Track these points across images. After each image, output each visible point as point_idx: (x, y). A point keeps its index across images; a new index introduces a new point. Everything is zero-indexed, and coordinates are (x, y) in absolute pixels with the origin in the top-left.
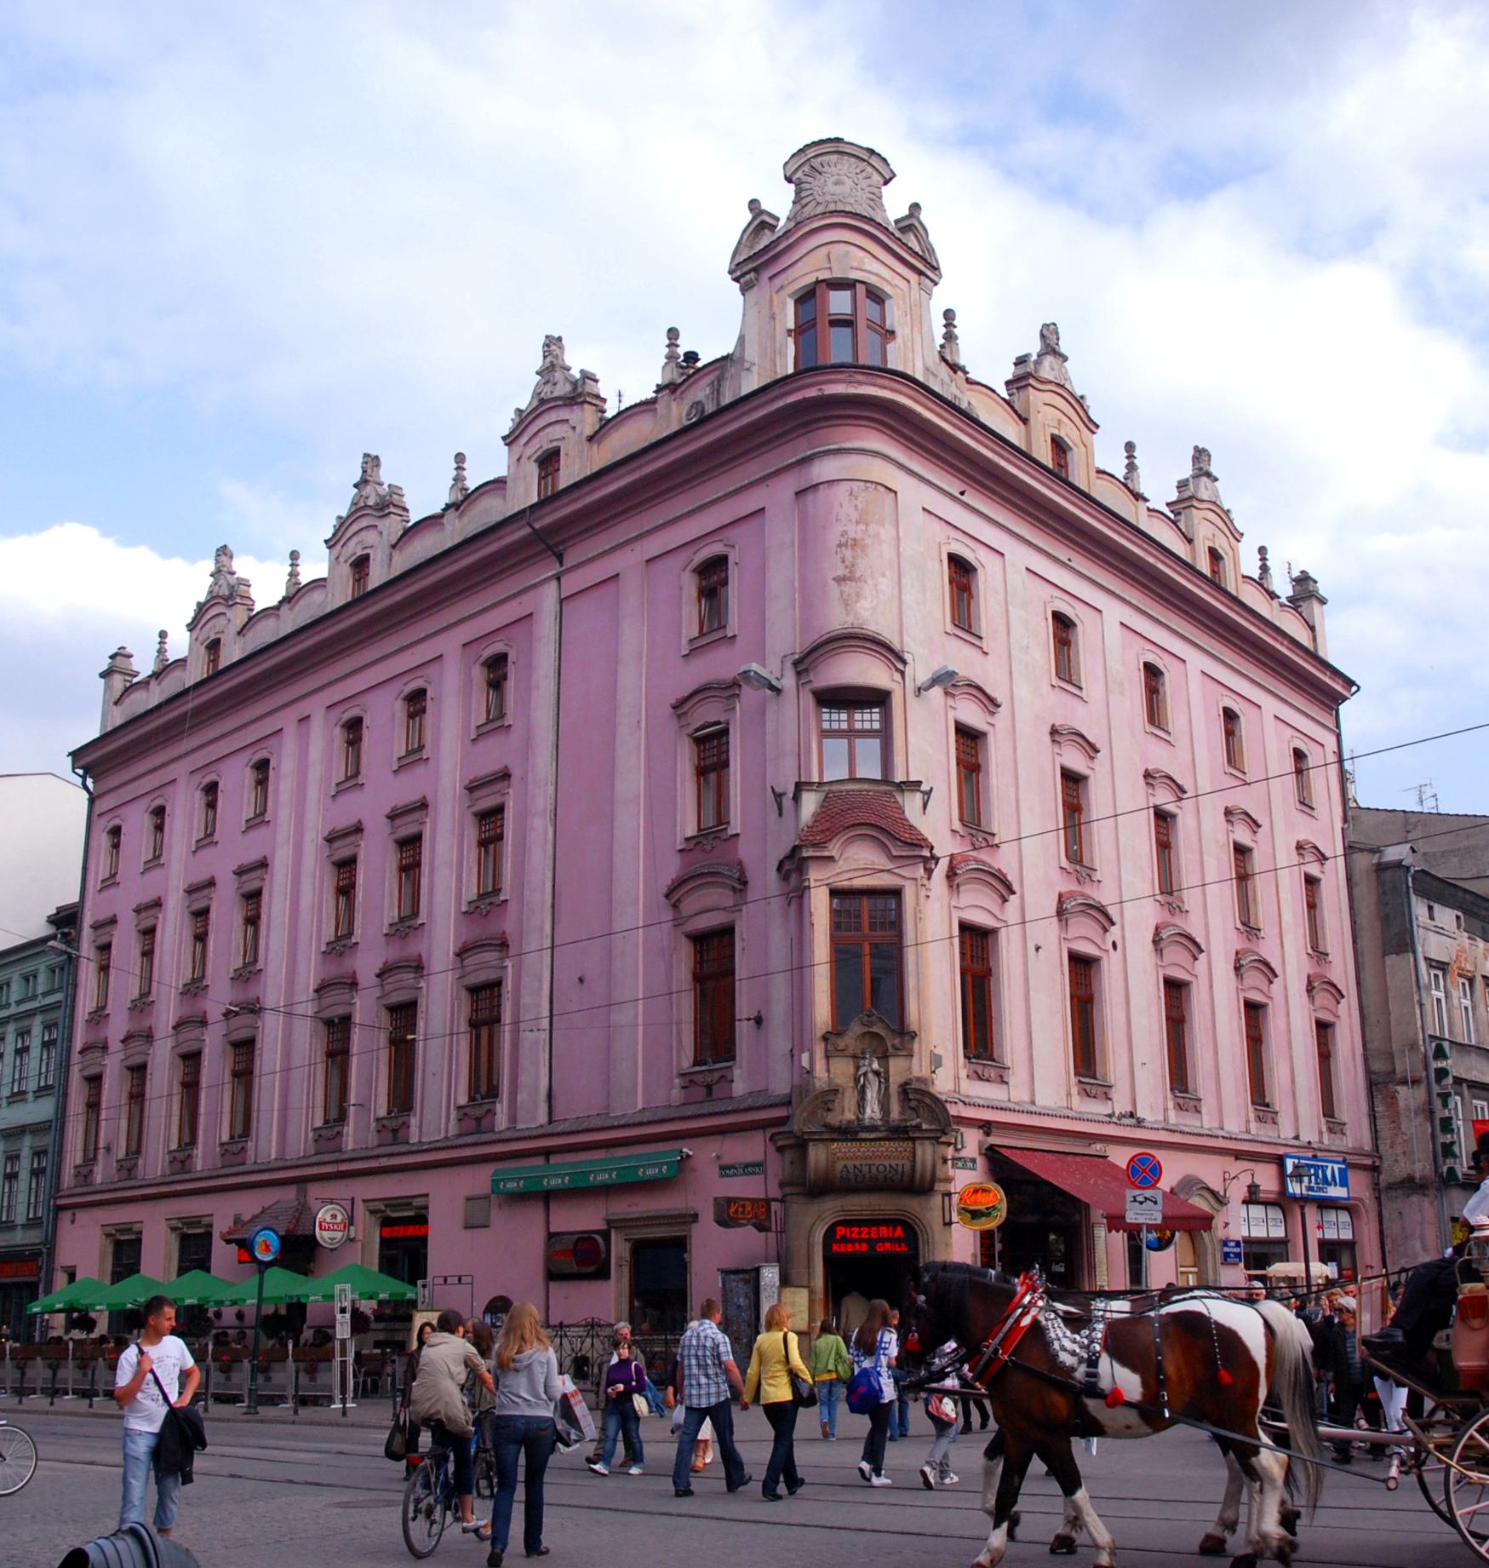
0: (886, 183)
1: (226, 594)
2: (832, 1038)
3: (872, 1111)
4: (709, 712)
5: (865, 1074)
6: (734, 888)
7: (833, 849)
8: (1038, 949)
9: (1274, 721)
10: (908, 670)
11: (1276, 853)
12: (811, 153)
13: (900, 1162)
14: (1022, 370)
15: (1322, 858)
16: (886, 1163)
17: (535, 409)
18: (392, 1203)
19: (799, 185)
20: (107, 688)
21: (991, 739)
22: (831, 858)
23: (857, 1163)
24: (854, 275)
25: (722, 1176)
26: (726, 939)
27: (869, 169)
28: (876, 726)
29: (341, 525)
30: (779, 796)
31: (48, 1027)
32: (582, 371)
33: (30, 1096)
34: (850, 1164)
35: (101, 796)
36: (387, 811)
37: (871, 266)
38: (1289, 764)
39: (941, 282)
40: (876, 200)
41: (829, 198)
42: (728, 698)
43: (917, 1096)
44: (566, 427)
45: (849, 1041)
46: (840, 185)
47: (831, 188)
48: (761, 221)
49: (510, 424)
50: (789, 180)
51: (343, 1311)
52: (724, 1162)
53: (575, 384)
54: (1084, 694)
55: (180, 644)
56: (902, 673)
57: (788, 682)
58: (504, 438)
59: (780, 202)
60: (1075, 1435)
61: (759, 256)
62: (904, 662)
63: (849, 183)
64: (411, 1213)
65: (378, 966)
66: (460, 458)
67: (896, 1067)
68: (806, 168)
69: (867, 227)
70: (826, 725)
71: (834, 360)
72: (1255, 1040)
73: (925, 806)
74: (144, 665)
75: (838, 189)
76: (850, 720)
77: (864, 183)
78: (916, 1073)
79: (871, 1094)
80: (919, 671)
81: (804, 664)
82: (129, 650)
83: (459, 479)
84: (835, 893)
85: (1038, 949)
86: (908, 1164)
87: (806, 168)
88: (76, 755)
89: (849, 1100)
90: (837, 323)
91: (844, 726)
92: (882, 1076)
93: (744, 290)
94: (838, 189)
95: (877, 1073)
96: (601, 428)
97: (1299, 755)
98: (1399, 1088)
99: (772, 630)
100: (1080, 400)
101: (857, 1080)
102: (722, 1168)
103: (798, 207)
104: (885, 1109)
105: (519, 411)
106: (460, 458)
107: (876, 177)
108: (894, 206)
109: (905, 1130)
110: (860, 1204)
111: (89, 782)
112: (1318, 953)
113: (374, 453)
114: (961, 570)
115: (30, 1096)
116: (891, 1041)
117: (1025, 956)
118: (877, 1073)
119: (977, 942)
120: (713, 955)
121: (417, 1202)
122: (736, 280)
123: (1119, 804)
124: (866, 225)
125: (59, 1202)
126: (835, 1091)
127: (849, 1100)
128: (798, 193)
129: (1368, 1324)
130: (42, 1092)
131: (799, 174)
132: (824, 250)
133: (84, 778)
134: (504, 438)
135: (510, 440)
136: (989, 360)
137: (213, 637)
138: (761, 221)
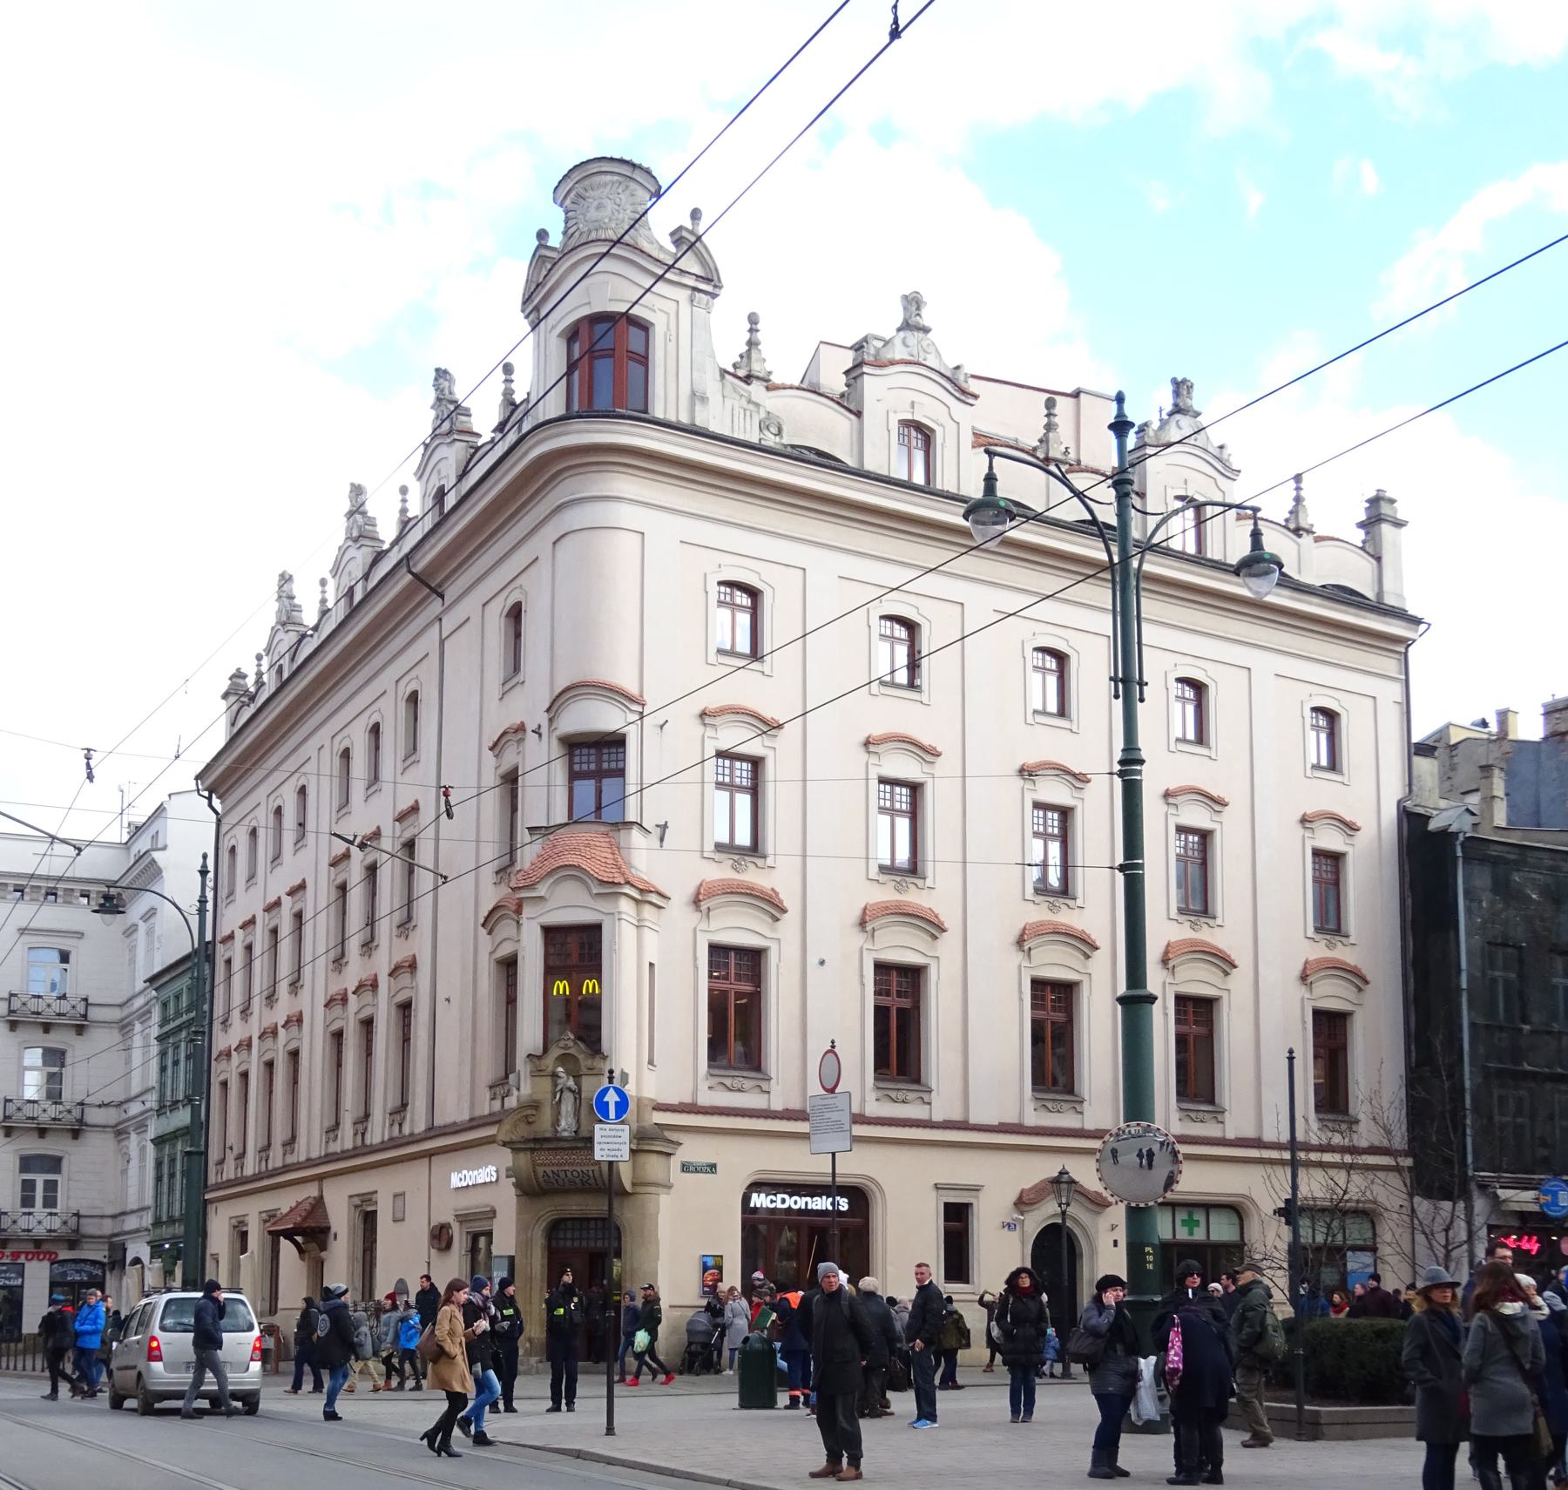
7: (542, 890)
12: (576, 176)
23: (555, 1169)
27: (633, 185)
34: (548, 1169)
35: (226, 813)
39: (723, 292)
41: (591, 226)
45: (549, 1061)
46: (610, 210)
51: (137, 1261)
54: (925, 699)
60: (863, 1416)
63: (609, 205)
66: (753, 320)
70: (577, 768)
73: (662, 840)
76: (599, 761)
79: (567, 1106)
89: (547, 1113)
91: (593, 767)
92: (577, 1093)
107: (642, 195)
108: (663, 221)
110: (576, 1206)
111: (216, 802)
116: (585, 1062)
127: (547, 1113)
129: (352, 1362)
133: (210, 799)
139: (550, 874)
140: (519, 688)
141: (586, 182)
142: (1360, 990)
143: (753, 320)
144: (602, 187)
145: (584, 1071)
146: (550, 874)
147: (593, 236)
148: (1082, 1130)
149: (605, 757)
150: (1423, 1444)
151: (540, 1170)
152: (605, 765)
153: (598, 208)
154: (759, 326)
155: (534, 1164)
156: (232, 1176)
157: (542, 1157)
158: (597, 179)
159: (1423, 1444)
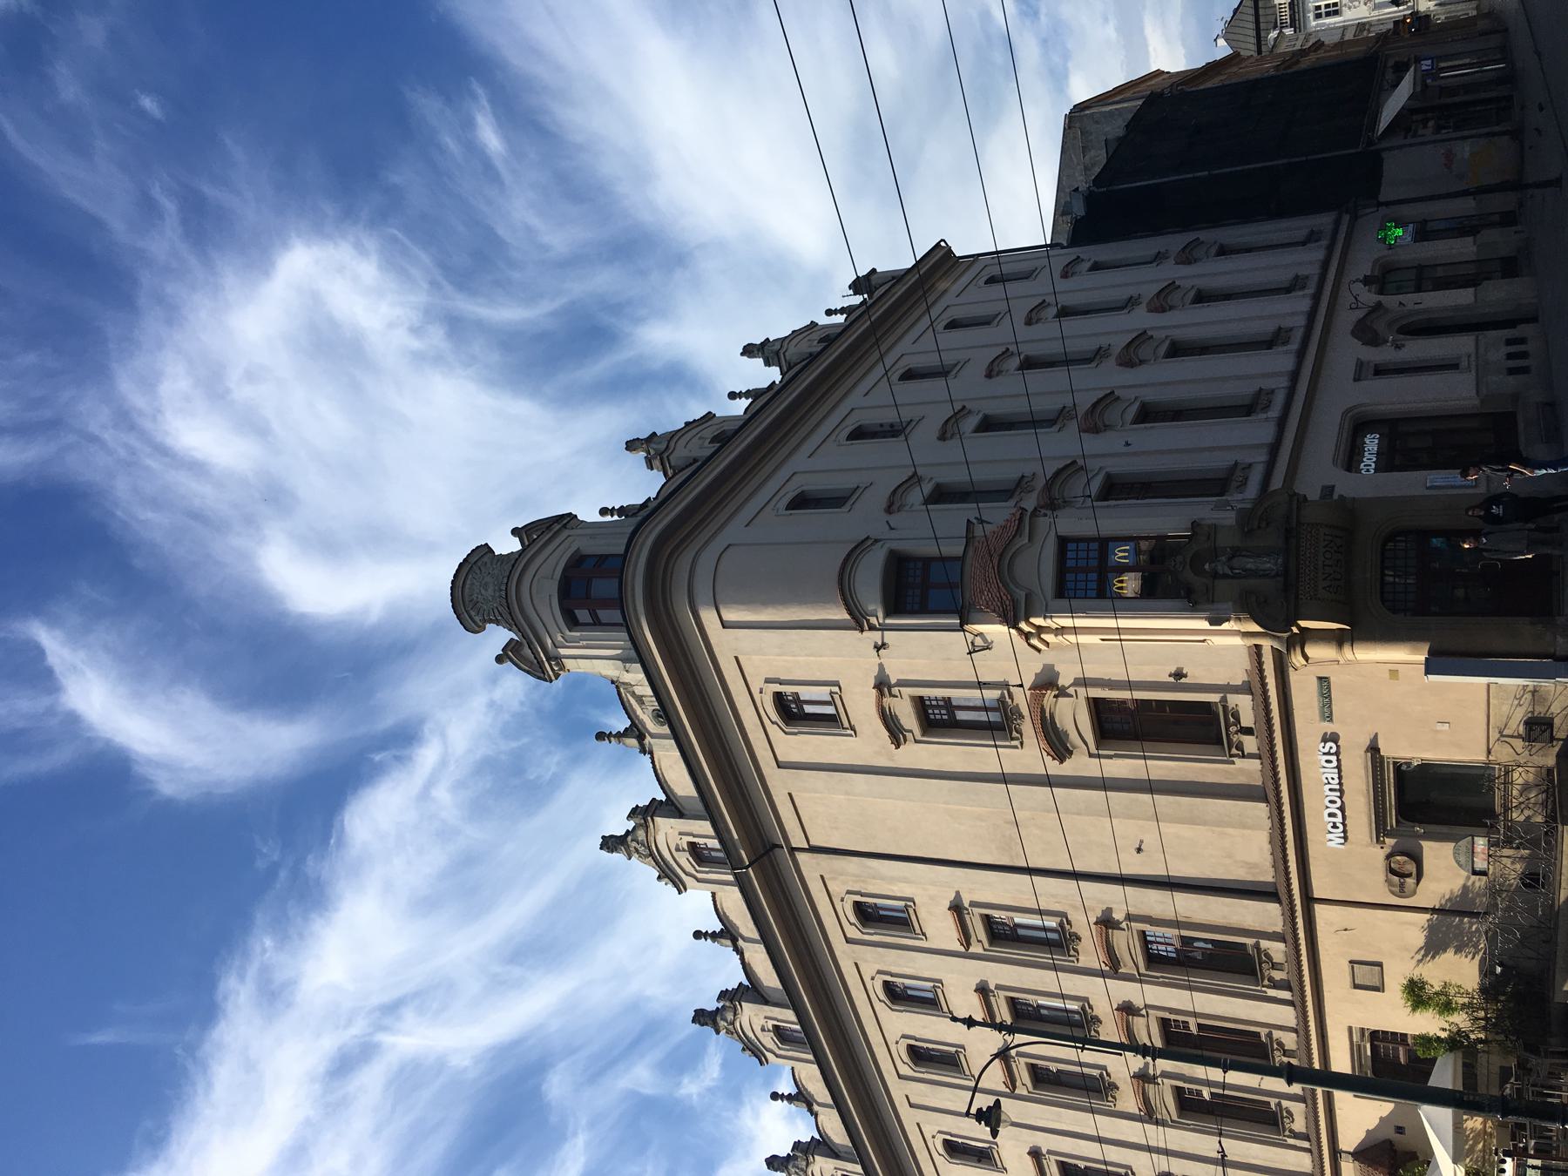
3: (1268, 564)
5: (1232, 569)
8: (1127, 444)
10: (874, 535)
15: (1078, 260)
19: (485, 621)
21: (941, 480)
32: (629, 817)
37: (554, 561)
38: (999, 287)
43: (1249, 521)
56: (876, 541)
59: (499, 636)
66: (698, 935)
72: (1227, 296)
83: (714, 936)
85: (1127, 444)
92: (1236, 552)
95: (1230, 559)
97: (991, 280)
98: (1423, 843)
100: (687, 424)
101: (1234, 577)
106: (698, 935)
107: (485, 559)
112: (1159, 258)
114: (802, 502)
117: (1135, 454)
119: (1115, 489)
123: (1009, 395)
128: (491, 621)
131: (477, 619)
135: (680, 887)
139: (1005, 585)
146: (1005, 585)
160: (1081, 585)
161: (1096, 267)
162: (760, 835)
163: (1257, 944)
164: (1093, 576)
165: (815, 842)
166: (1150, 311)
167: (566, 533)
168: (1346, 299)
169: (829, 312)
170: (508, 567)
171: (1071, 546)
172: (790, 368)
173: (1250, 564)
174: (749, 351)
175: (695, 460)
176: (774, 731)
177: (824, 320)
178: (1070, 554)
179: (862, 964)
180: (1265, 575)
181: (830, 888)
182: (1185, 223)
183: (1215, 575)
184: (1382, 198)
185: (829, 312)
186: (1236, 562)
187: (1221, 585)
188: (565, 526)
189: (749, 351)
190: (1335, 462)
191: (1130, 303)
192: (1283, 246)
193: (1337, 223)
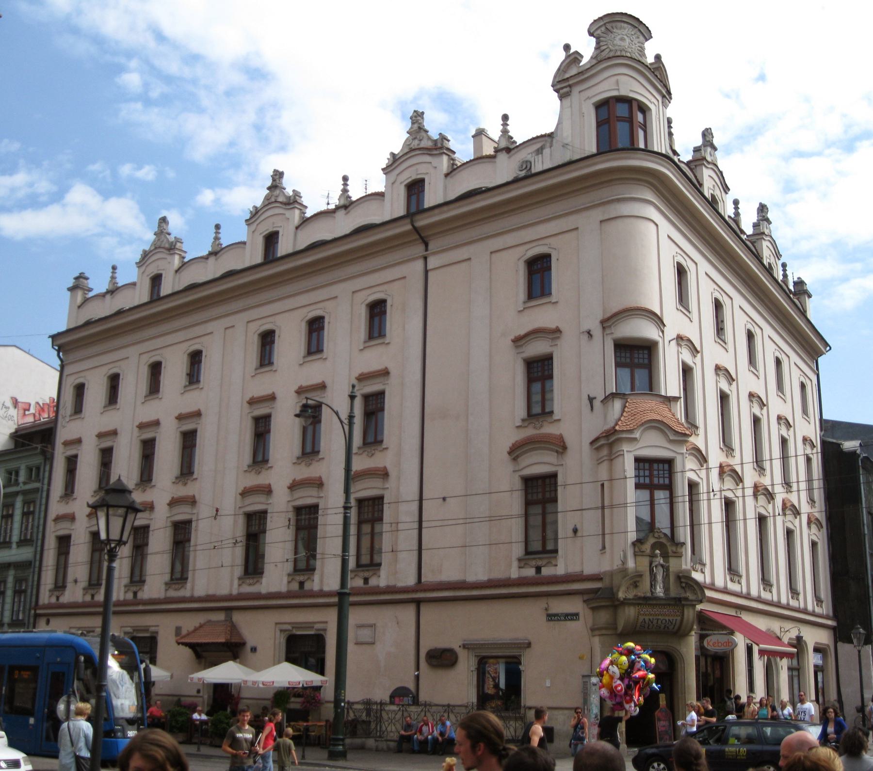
0: (647, 40)
1: (164, 244)
2: (639, 544)
3: (659, 591)
4: (537, 348)
6: (557, 452)
7: (637, 435)
9: (795, 368)
11: (797, 448)
13: (675, 618)
14: (698, 156)
15: (813, 446)
16: (667, 618)
17: (406, 154)
18: (136, 629)
19: (598, 38)
20: (73, 299)
22: (635, 439)
23: (651, 618)
24: (632, 95)
25: (549, 620)
26: (553, 480)
27: (639, 33)
28: (636, 361)
29: (257, 213)
30: (591, 400)
31: (26, 503)
33: (14, 545)
34: (647, 618)
36: (296, 388)
40: (642, 51)
41: (617, 48)
42: (553, 339)
44: (428, 166)
45: (647, 547)
46: (623, 39)
47: (617, 42)
48: (573, 58)
49: (387, 161)
50: (591, 34)
52: (550, 612)
53: (435, 141)
55: (128, 275)
56: (663, 332)
57: (597, 332)
58: (383, 170)
59: (586, 48)
61: (568, 79)
62: (664, 325)
63: (628, 40)
64: (312, 632)
65: (288, 482)
66: (345, 179)
67: (673, 563)
68: (603, 29)
69: (630, 63)
71: (620, 146)
74: (99, 284)
75: (623, 44)
76: (631, 358)
77: (636, 41)
78: (684, 567)
80: (671, 332)
81: (607, 323)
82: (87, 275)
84: (638, 460)
86: (679, 618)
87: (603, 29)
88: (54, 337)
90: (621, 119)
92: (666, 569)
93: (561, 98)
94: (623, 44)
95: (662, 566)
96: (451, 172)
99: (574, 303)
100: (721, 173)
102: (549, 615)
103: (598, 51)
104: (666, 589)
105: (393, 155)
109: (679, 600)
113: (281, 170)
115: (14, 545)
116: (671, 549)
118: (662, 566)
120: (540, 492)
121: (317, 626)
122: (556, 91)
124: (637, 64)
125: (38, 612)
126: (641, 576)
128: (598, 43)
130: (22, 543)
131: (599, 32)
132: (614, 79)
134: (383, 170)
136: (685, 145)
137: (156, 272)
138: (573, 58)
139: (642, 424)
140: (550, 306)
141: (614, 24)
142: (387, 448)
143: (345, 179)
144: (617, 32)
145: (671, 554)
146: (642, 424)
147: (618, 53)
148: (464, 582)
149: (636, 355)
150: (153, 679)
151: (641, 618)
152: (636, 361)
153: (622, 39)
154: (348, 183)
155: (639, 614)
156: (122, 598)
157: (646, 610)
158: (619, 24)
159: (153, 679)
160: (642, 473)
161: (809, 460)
162: (435, 234)
163: (351, 571)
164: (647, 481)
165: (430, 274)
166: (783, 501)
167: (660, 99)
168: (788, 625)
169: (736, 203)
170: (636, 56)
171: (666, 466)
172: (753, 243)
173: (659, 578)
174: (707, 134)
175: (701, 185)
176: (520, 251)
177: (729, 200)
178: (661, 466)
179: (343, 306)
180: (653, 586)
181: (398, 281)
182: (831, 516)
183: (653, 556)
184: (839, 644)
185: (736, 203)
186: (661, 570)
187: (645, 561)
188: (664, 96)
189: (707, 134)
190: (816, 643)
191: (727, 446)
192: (180, 343)
193: (827, 617)
